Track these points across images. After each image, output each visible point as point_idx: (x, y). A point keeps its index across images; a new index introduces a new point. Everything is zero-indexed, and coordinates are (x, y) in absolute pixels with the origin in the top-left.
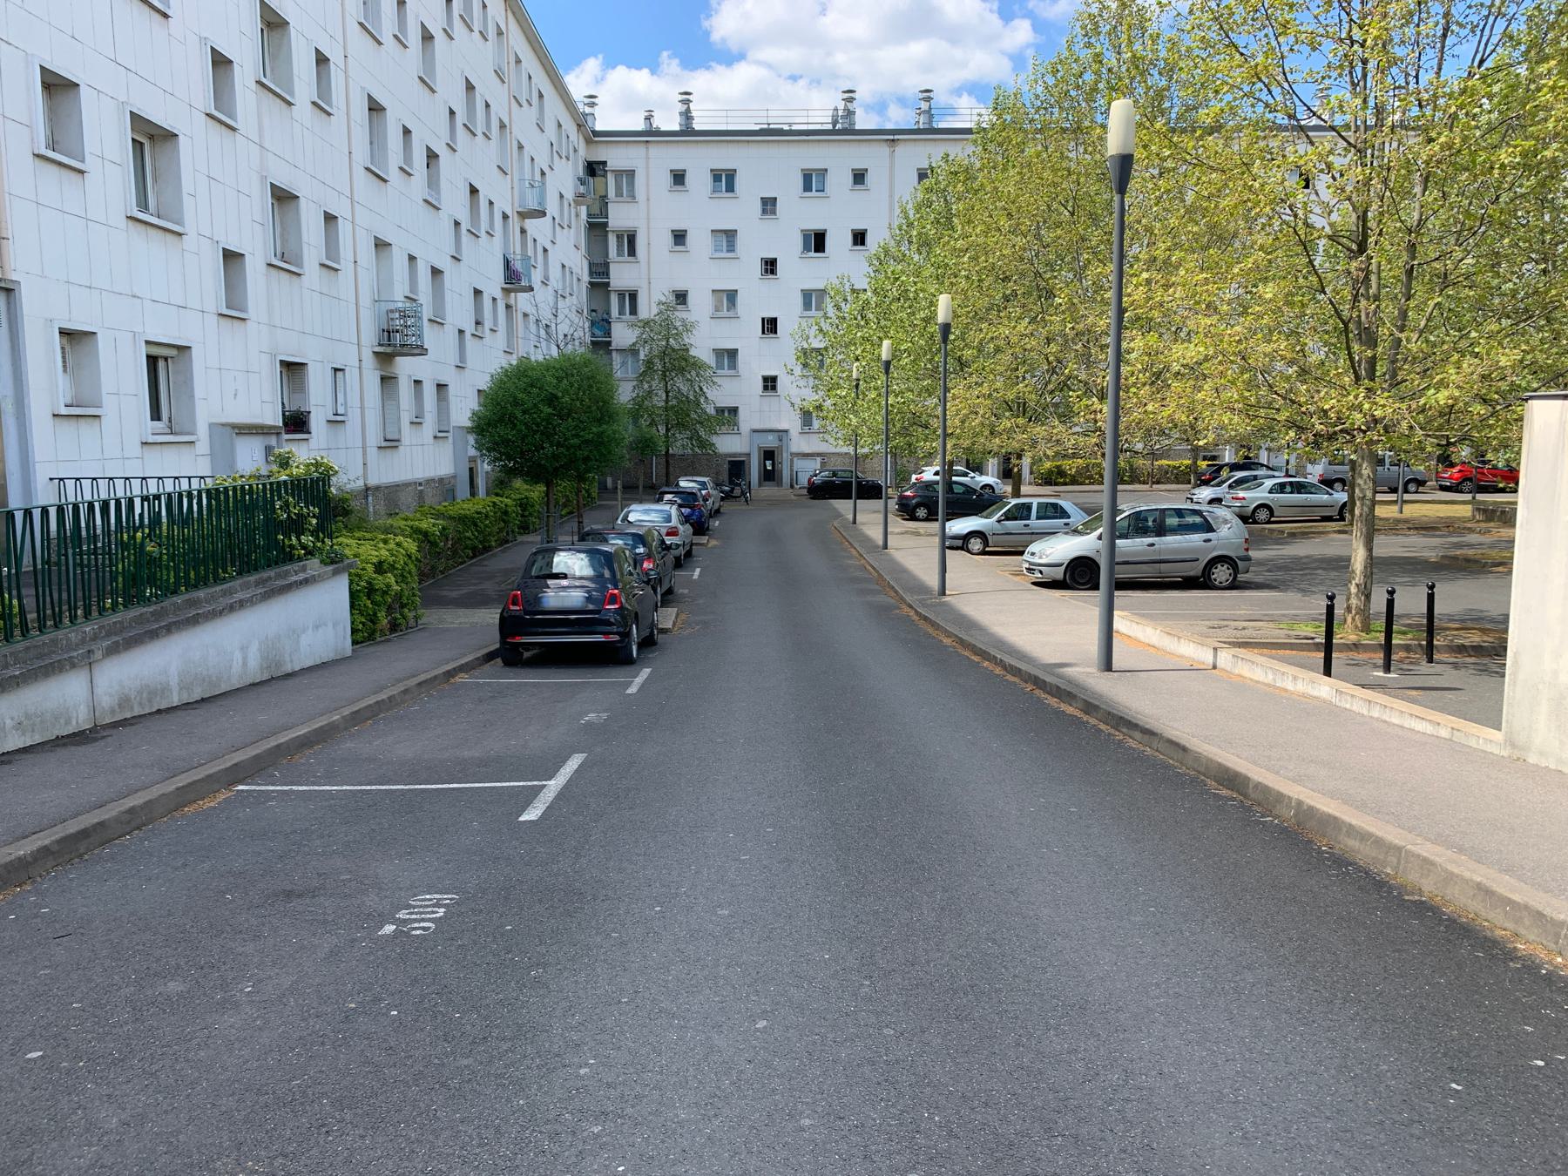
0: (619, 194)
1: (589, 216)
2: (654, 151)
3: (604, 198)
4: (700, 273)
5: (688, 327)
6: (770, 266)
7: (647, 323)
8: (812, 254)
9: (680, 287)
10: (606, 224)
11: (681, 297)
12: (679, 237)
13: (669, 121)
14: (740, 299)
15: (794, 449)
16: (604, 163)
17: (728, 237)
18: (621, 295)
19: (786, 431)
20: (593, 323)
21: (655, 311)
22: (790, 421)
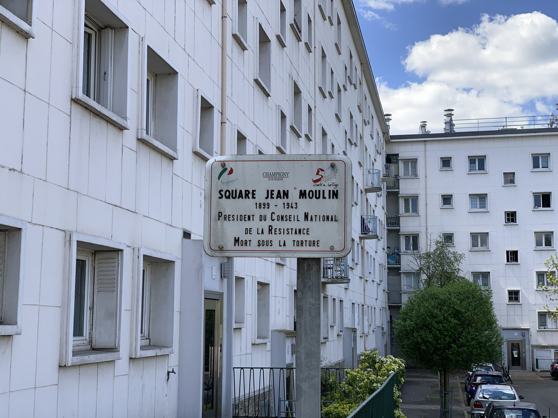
0: (406, 173)
1: (387, 188)
2: (429, 146)
3: (397, 176)
4: (462, 223)
5: (458, 258)
6: (511, 217)
7: (428, 255)
8: (541, 208)
9: (448, 230)
10: (398, 193)
11: (449, 238)
12: (447, 200)
13: (437, 126)
14: (491, 239)
15: (534, 342)
16: (397, 155)
17: (480, 199)
18: (407, 237)
19: (528, 330)
20: (388, 256)
21: (434, 247)
22: (530, 322)
